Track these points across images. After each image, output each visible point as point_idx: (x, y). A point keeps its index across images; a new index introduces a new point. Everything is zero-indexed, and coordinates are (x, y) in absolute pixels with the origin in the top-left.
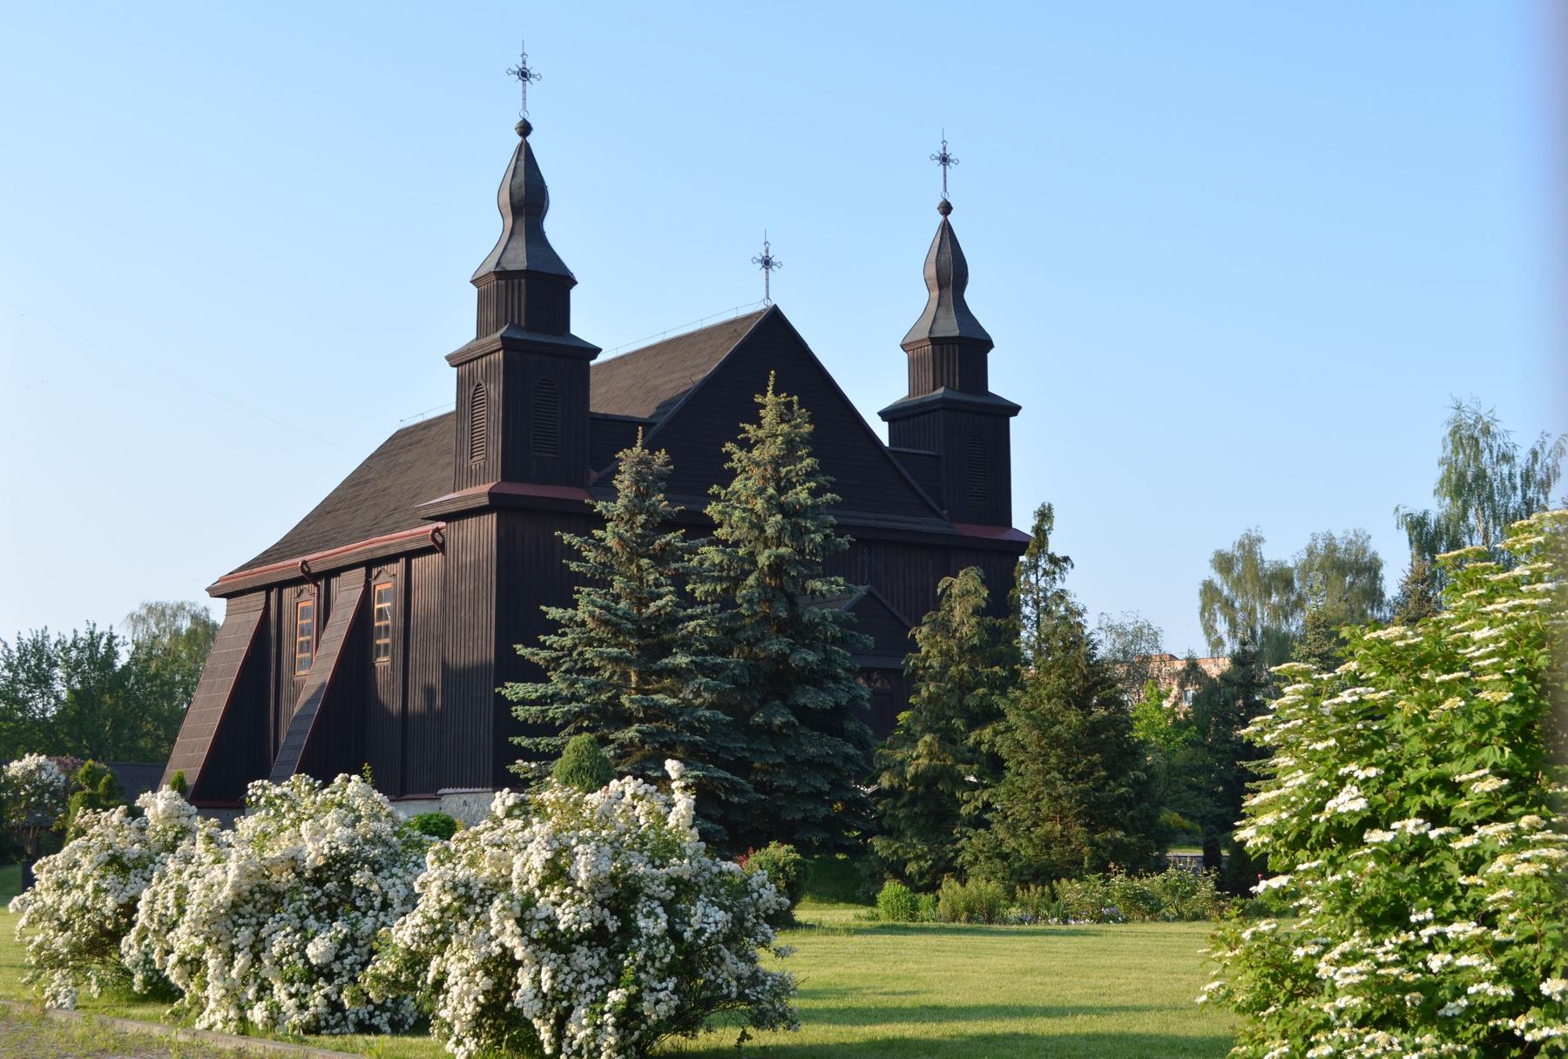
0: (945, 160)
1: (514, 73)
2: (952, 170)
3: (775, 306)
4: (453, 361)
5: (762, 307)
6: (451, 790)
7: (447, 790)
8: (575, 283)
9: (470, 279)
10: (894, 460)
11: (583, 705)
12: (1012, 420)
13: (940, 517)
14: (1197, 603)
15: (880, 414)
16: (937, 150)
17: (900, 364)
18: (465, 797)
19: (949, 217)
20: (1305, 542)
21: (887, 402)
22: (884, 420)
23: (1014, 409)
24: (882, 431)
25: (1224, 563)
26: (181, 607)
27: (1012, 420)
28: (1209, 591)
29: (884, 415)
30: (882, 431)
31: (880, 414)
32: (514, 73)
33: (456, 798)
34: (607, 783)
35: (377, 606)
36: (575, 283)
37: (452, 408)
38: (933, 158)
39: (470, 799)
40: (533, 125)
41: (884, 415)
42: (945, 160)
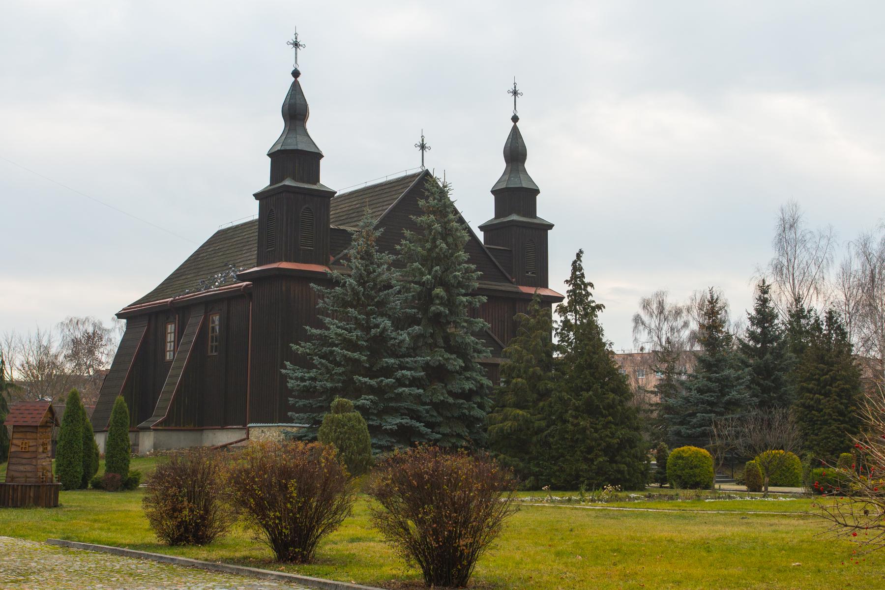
0: (296, 45)
1: (291, 44)
4: (257, 196)
5: (420, 170)
6: (255, 425)
9: (267, 153)
10: (490, 254)
12: (549, 231)
13: (511, 282)
14: (633, 325)
16: (292, 38)
17: (490, 201)
20: (690, 294)
21: (482, 222)
22: (257, 199)
23: (551, 226)
24: (480, 236)
25: (646, 305)
26: (87, 319)
27: (549, 231)
28: (638, 320)
29: (481, 228)
30: (480, 236)
31: (254, 195)
32: (291, 44)
34: (304, 368)
35: (211, 325)
37: (257, 217)
39: (265, 430)
41: (481, 228)
42: (296, 45)
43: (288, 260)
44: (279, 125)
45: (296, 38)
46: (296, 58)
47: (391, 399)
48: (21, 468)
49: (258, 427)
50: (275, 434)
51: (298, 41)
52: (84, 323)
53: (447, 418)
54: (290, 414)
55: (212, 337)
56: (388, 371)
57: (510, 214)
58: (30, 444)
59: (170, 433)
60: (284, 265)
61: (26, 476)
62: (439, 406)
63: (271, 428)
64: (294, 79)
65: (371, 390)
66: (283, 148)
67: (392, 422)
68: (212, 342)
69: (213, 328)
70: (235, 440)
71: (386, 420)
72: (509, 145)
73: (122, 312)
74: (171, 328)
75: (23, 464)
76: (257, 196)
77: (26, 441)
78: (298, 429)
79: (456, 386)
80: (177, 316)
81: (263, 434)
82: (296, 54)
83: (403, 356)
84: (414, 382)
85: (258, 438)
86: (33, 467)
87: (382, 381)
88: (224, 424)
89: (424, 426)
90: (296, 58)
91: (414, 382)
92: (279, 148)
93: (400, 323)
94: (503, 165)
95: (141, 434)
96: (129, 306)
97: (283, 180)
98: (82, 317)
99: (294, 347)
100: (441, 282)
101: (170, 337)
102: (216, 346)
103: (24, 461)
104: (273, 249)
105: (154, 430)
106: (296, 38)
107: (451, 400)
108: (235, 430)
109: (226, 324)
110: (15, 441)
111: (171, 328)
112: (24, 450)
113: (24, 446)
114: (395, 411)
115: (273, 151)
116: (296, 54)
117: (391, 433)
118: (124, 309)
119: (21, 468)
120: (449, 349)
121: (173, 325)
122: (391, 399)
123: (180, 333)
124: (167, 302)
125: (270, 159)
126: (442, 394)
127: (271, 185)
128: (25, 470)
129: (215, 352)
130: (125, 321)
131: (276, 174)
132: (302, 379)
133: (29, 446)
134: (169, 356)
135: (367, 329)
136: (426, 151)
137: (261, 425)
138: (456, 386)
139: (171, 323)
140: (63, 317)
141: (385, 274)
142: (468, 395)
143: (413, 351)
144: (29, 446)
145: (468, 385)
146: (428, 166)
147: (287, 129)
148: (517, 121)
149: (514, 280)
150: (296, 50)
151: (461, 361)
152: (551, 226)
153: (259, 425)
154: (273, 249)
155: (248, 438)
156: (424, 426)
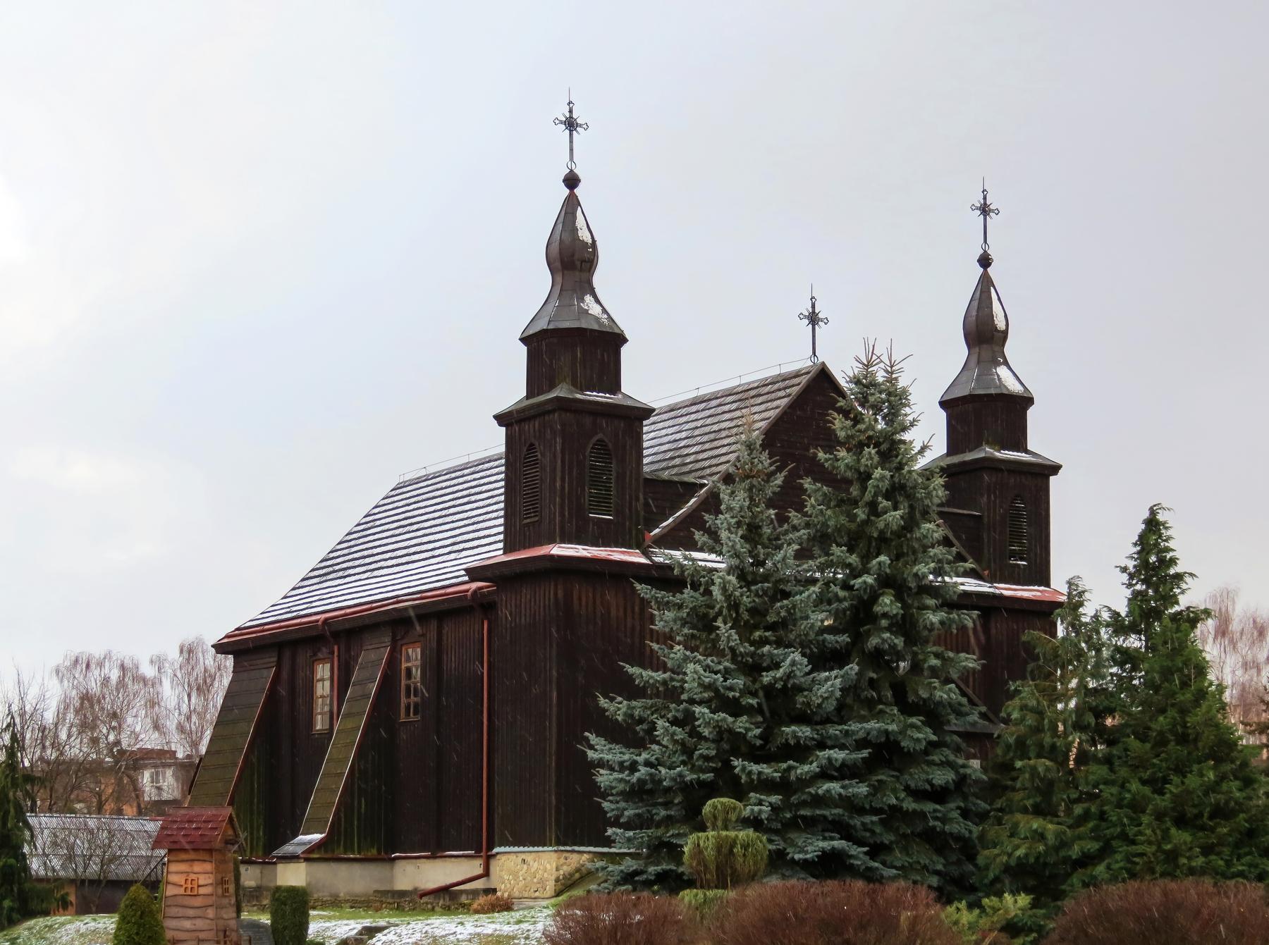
1: (561, 122)
2: (993, 220)
3: (823, 363)
4: (501, 419)
6: (507, 849)
7: (502, 849)
8: (625, 340)
11: (1234, 766)
12: (1052, 478)
15: (496, 417)
18: (523, 856)
19: (988, 269)
22: (500, 425)
23: (1055, 469)
26: (108, 656)
27: (1052, 478)
31: (496, 417)
32: (561, 122)
33: (513, 857)
35: (404, 666)
36: (625, 340)
38: (973, 208)
39: (529, 858)
40: (581, 177)
43: (566, 539)
44: (541, 282)
45: (571, 111)
46: (571, 150)
47: (804, 804)
48: (187, 924)
49: (531, 852)
50: (548, 866)
51: (574, 116)
52: (101, 665)
53: (904, 836)
54: (610, 831)
55: (408, 687)
56: (800, 752)
57: (977, 445)
58: (201, 882)
59: (334, 866)
60: (558, 550)
61: (198, 937)
62: (893, 815)
63: (540, 854)
64: (567, 191)
65: (767, 786)
66: (551, 327)
67: (813, 846)
68: (408, 696)
69: (409, 670)
70: (460, 878)
71: (792, 840)
72: (974, 313)
73: (226, 640)
74: (323, 671)
75: (189, 918)
76: (501, 419)
77: (193, 876)
78: (591, 855)
79: (917, 776)
80: (336, 648)
81: (525, 866)
82: (571, 142)
83: (827, 720)
84: (844, 772)
85: (515, 875)
86: (208, 921)
87: (790, 768)
88: (436, 848)
89: (866, 853)
90: (571, 150)
91: (844, 772)
92: (542, 325)
93: (824, 659)
94: (964, 351)
95: (280, 867)
96: (238, 629)
97: (552, 387)
98: (97, 651)
99: (603, 702)
100: (887, 582)
101: (323, 688)
102: (416, 705)
103: (191, 912)
104: (537, 519)
105: (307, 860)
106: (571, 111)
107: (910, 805)
108: (459, 859)
109: (434, 664)
110: (173, 878)
111: (323, 671)
112: (189, 892)
113: (190, 886)
114: (811, 825)
115: (531, 332)
116: (571, 142)
117: (806, 866)
118: (227, 636)
119: (187, 924)
120: (908, 708)
121: (328, 666)
122: (804, 804)
123: (342, 683)
124: (317, 621)
125: (525, 349)
126: (894, 791)
127: (528, 397)
128: (193, 927)
129: (415, 713)
130: (231, 657)
131: (537, 377)
132: (633, 767)
133: (199, 886)
134: (320, 724)
135: (753, 668)
136: (820, 327)
137: (521, 849)
138: (917, 776)
139: (323, 660)
140: (59, 657)
141: (783, 561)
142: (939, 795)
143: (842, 713)
144: (199, 886)
145: (942, 777)
146: (823, 357)
147: (558, 288)
148: (989, 265)
149: (986, 572)
150: (571, 135)
151: (928, 730)
152: (1055, 469)
153: (516, 849)
154: (537, 519)
155: (486, 874)
156: (866, 853)
